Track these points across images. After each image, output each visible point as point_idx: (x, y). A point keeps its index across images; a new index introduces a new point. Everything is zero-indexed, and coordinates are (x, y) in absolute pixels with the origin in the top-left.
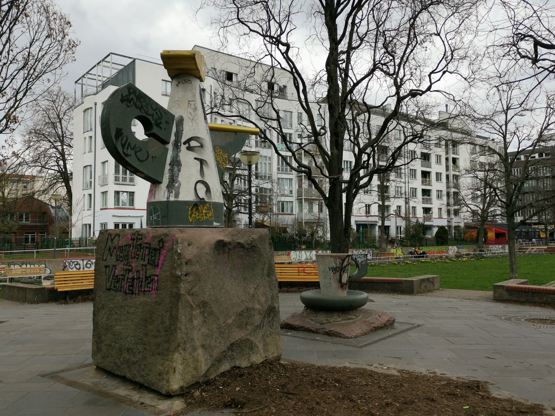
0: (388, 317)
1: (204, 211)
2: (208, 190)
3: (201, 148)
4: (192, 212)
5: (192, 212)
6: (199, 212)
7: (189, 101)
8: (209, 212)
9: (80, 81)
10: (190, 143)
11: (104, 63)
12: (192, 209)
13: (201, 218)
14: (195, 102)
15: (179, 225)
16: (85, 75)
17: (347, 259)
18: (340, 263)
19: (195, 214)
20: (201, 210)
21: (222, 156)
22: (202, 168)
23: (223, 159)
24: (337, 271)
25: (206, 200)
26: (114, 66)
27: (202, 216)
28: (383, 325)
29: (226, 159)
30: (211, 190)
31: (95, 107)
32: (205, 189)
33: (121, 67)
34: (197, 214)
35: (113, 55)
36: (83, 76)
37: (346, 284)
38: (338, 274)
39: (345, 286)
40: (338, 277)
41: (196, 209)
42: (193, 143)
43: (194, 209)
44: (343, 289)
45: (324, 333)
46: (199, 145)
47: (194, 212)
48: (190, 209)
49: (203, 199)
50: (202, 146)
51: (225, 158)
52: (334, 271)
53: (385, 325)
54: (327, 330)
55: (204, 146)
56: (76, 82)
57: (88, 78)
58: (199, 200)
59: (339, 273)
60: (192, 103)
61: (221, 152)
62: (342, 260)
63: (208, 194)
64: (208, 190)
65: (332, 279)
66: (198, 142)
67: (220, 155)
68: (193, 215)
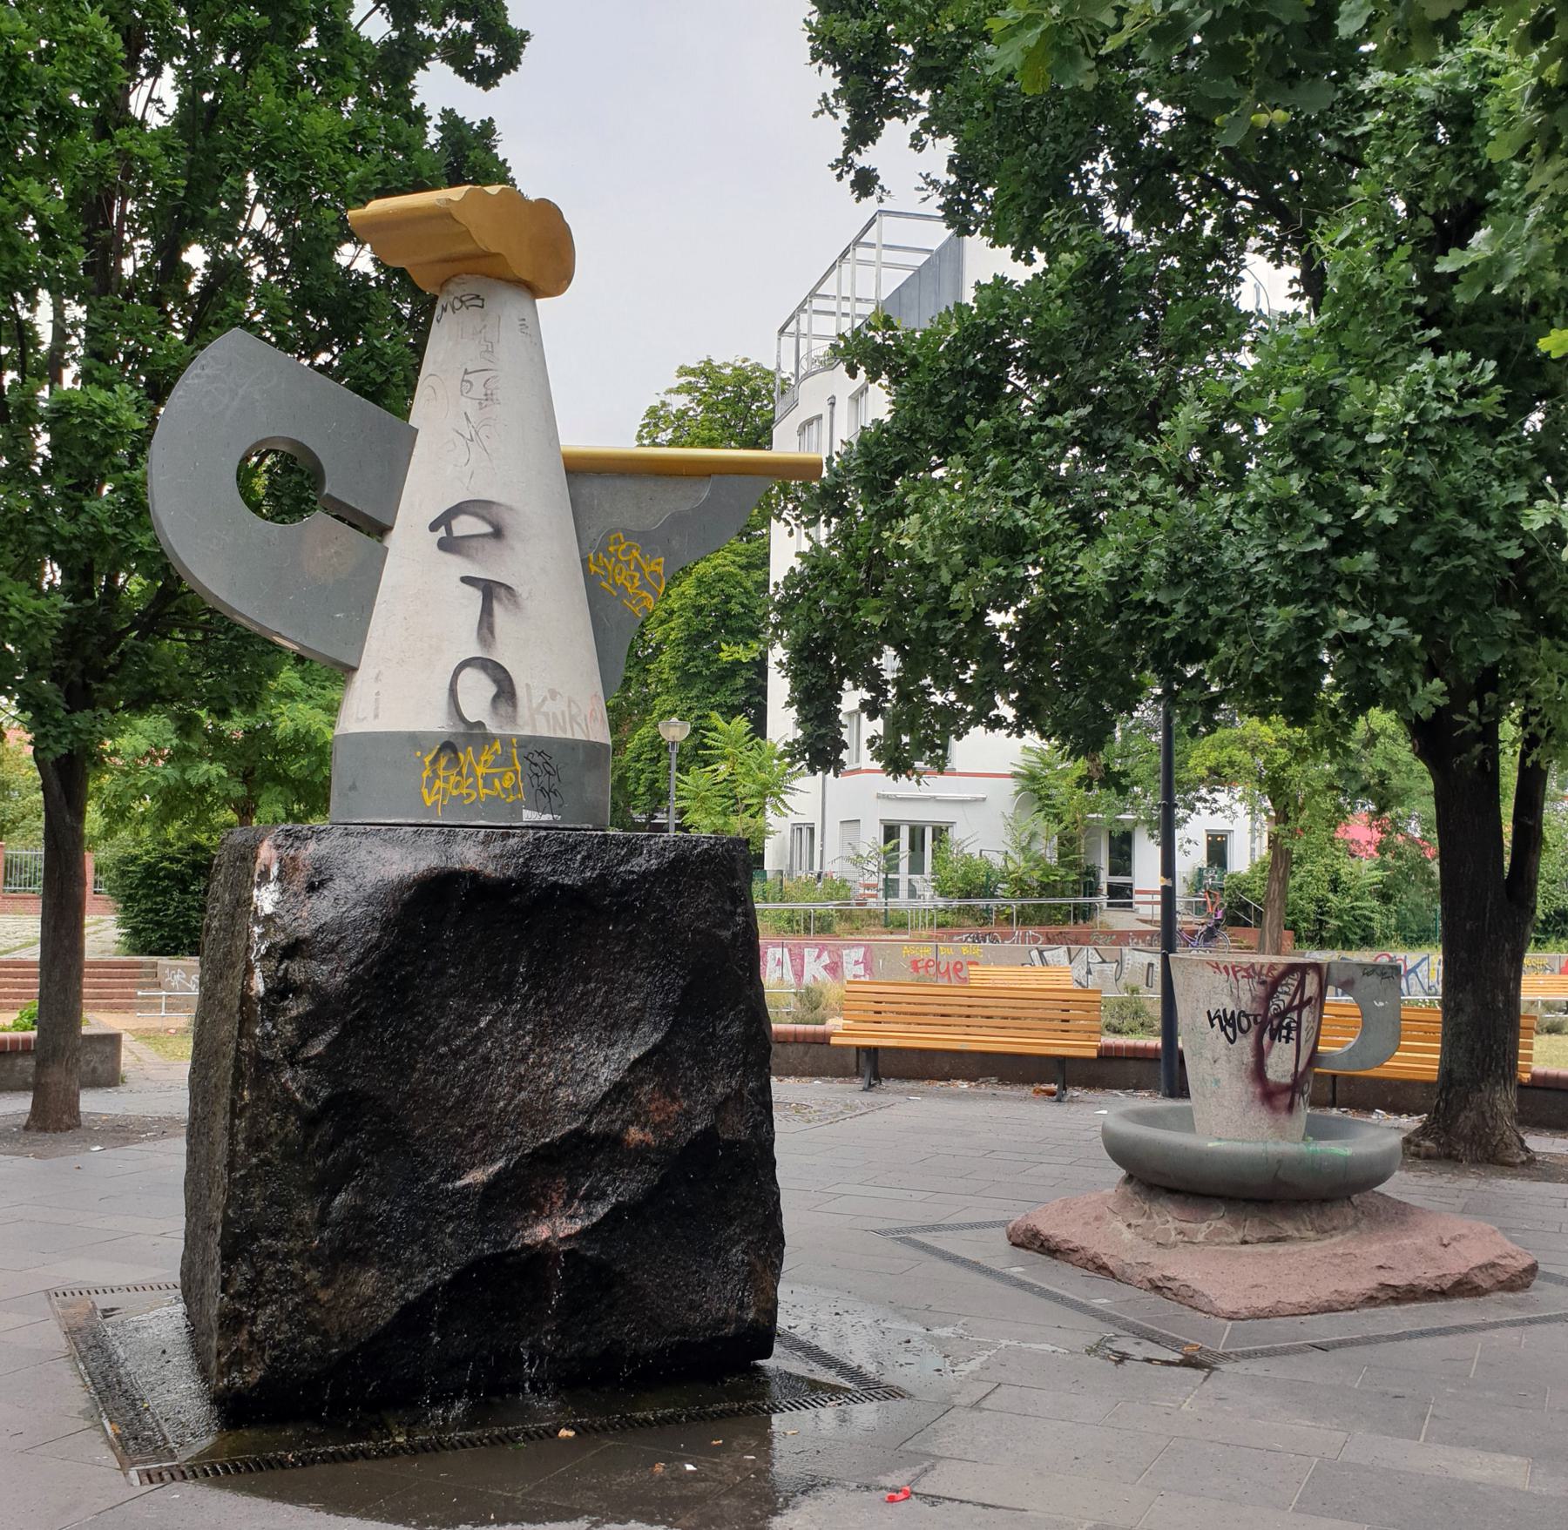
1: (480, 770)
2: (505, 691)
3: (490, 544)
4: (434, 771)
6: (460, 773)
7: (466, 372)
8: (503, 773)
9: (791, 328)
10: (455, 523)
11: (861, 253)
12: (435, 760)
13: (469, 795)
14: (487, 375)
15: (390, 817)
17: (1293, 981)
18: (1254, 999)
19: (446, 779)
20: (470, 764)
21: (638, 568)
22: (487, 612)
23: (642, 578)
24: (1243, 1031)
25: (492, 728)
26: (888, 255)
27: (474, 786)
28: (1447, 1284)
29: (658, 579)
30: (520, 691)
31: (832, 413)
32: (492, 690)
33: (920, 259)
34: (453, 779)
35: (886, 219)
36: (801, 309)
38: (1246, 1043)
40: (1249, 1058)
41: (449, 761)
42: (465, 526)
43: (443, 762)
44: (1274, 1109)
46: (487, 529)
47: (441, 773)
48: (428, 760)
49: (480, 724)
50: (498, 533)
51: (652, 573)
52: (1229, 1030)
53: (1459, 1283)
54: (1154, 1275)
55: (507, 532)
56: (782, 331)
57: (816, 312)
58: (461, 729)
59: (1251, 1037)
61: (636, 554)
62: (1263, 983)
63: (504, 708)
64: (505, 691)
65: (1223, 1061)
66: (483, 518)
67: (628, 563)
68: (439, 784)
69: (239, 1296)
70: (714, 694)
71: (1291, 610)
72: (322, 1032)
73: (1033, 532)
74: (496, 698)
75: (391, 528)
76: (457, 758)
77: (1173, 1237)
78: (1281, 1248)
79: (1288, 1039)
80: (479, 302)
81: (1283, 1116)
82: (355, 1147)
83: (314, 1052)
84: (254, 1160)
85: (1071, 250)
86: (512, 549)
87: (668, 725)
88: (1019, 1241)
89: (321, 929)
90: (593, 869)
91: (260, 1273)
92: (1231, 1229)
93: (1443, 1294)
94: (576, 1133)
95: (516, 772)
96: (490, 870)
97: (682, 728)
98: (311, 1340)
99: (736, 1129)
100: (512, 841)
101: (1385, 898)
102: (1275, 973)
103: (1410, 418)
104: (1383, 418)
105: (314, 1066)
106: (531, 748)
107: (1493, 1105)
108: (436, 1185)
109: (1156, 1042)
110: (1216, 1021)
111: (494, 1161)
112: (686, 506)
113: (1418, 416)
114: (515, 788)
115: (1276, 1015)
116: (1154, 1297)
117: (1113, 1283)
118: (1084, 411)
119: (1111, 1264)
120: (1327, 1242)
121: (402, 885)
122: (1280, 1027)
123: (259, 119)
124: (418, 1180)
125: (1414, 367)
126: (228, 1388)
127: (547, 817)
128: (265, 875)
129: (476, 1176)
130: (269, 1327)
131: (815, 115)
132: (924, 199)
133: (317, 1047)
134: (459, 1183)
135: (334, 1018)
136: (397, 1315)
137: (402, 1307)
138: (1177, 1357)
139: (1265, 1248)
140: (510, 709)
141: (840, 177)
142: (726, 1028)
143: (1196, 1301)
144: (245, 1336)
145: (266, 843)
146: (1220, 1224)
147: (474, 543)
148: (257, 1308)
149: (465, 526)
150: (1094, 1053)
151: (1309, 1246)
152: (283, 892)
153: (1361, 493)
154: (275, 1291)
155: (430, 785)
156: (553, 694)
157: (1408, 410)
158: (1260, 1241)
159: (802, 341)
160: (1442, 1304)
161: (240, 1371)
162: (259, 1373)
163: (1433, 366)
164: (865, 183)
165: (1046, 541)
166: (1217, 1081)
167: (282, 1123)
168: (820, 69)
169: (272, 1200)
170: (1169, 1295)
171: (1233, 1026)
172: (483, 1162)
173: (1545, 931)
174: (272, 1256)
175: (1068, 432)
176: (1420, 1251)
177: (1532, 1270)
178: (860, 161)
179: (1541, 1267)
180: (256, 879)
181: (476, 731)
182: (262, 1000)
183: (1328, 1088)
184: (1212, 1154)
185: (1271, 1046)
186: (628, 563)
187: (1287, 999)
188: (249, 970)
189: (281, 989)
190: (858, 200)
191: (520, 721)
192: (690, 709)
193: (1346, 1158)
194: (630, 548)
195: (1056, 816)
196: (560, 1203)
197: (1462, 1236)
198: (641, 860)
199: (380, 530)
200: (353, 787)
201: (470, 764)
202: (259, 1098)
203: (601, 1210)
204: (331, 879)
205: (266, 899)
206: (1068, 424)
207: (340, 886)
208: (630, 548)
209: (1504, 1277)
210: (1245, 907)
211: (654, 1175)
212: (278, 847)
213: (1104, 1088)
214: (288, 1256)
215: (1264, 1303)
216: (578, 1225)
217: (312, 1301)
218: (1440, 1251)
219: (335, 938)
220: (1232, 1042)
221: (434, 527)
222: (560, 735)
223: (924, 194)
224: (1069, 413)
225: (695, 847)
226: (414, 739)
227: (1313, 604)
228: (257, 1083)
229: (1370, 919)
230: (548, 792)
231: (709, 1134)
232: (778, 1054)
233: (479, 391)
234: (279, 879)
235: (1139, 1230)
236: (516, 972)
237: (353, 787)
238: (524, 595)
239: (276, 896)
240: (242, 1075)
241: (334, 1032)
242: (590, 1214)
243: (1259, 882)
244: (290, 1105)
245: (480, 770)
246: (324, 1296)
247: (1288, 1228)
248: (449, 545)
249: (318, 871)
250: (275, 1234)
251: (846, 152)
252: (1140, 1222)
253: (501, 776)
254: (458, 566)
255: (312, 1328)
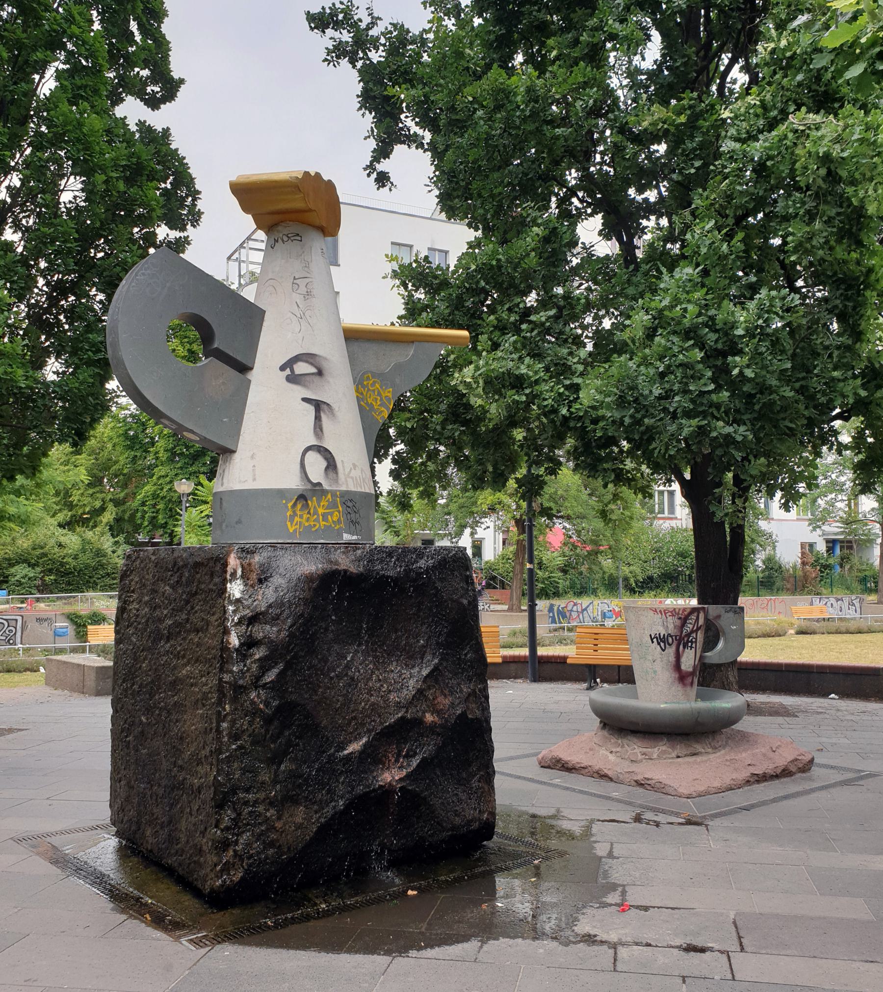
0: (797, 753)
1: (321, 511)
2: (331, 465)
3: (316, 379)
4: (294, 512)
5: (294, 512)
6: (309, 513)
7: (295, 279)
9: (234, 257)
10: (295, 367)
12: (295, 505)
13: (315, 525)
14: (307, 280)
15: (266, 539)
16: (244, 242)
17: (694, 617)
18: (675, 627)
19: (301, 516)
20: (315, 507)
21: (379, 394)
22: (318, 418)
23: (381, 400)
24: (670, 645)
25: (326, 486)
27: (317, 520)
28: (779, 771)
32: (324, 464)
34: (305, 516)
36: (241, 246)
37: (692, 674)
38: (671, 651)
39: (689, 680)
40: (672, 659)
41: (303, 506)
42: (301, 368)
43: (299, 506)
44: (684, 685)
45: (634, 783)
46: (314, 370)
47: (298, 513)
48: (290, 505)
49: (319, 484)
50: (320, 373)
51: (386, 397)
52: (662, 644)
53: (784, 770)
54: (639, 777)
55: (324, 372)
56: (229, 258)
57: (251, 249)
58: (309, 487)
59: (674, 647)
60: (302, 283)
61: (377, 386)
62: (680, 618)
63: (331, 474)
64: (331, 465)
66: (312, 364)
67: (374, 391)
68: (297, 519)
69: (227, 829)
70: (191, 465)
71: (695, 422)
72: (273, 667)
73: (529, 378)
74: (327, 469)
75: (251, 369)
76: (307, 505)
77: (640, 757)
78: (699, 759)
79: (691, 647)
80: (299, 238)
81: (689, 688)
82: (289, 735)
83: (270, 679)
84: (234, 747)
85: (538, 226)
86: (328, 382)
87: (181, 484)
88: (546, 765)
89: (270, 606)
90: (401, 567)
91: (239, 814)
92: (670, 750)
93: (777, 777)
94: (402, 718)
95: (339, 512)
96: (353, 569)
97: (188, 486)
98: (271, 851)
99: (474, 713)
100: (359, 552)
101: (564, 571)
102: (686, 613)
103: (760, 322)
104: (745, 322)
105: (269, 688)
106: (346, 498)
107: (727, 678)
108: (333, 754)
109: (525, 652)
110: (655, 640)
111: (361, 738)
112: (402, 360)
113: (764, 322)
114: (339, 521)
115: (686, 636)
116: (641, 790)
117: (612, 784)
118: (552, 312)
119: (610, 773)
120: (718, 754)
121: (309, 579)
122: (688, 641)
123: (58, 118)
124: (324, 752)
125: (758, 296)
126: (222, 886)
127: (355, 537)
128: (234, 574)
129: (354, 747)
130: (248, 845)
131: (365, 139)
132: (430, 191)
133: (271, 676)
134: (346, 752)
135: (281, 658)
136: (316, 833)
137: (318, 827)
138: (683, 821)
139: (691, 759)
140: (335, 475)
141: (369, 175)
142: (466, 655)
143: (667, 790)
144: (231, 853)
145: (232, 556)
146: (664, 748)
147: (308, 378)
148: (237, 835)
149: (301, 368)
150: (500, 660)
151: (711, 756)
152: (246, 585)
153: (735, 361)
154: (248, 824)
155: (292, 521)
156: (355, 466)
157: (759, 318)
158: (686, 756)
159: (242, 264)
160: (777, 782)
161: (229, 874)
162: (240, 875)
163: (769, 295)
164: (383, 179)
165: (537, 382)
166: (655, 672)
167: (251, 723)
168: (363, 115)
169: (244, 771)
170: (649, 788)
171: (664, 642)
172: (356, 739)
173: (642, 587)
174: (246, 803)
175: (543, 324)
176: (764, 755)
177: (812, 761)
178: (381, 167)
179: (816, 761)
180: (228, 577)
181: (317, 488)
182: (237, 650)
183: (616, 674)
184: (663, 711)
185: (684, 651)
186: (374, 391)
187: (691, 626)
188: (226, 632)
189: (249, 643)
190: (378, 189)
191: (340, 482)
192: (176, 475)
193: (729, 709)
194: (374, 383)
195: (395, 532)
196: (393, 760)
197: (780, 746)
198: (423, 561)
199: (244, 368)
200: (239, 522)
201: (315, 507)
202: (236, 709)
203: (415, 762)
204: (271, 576)
205: (235, 589)
206: (543, 319)
207: (277, 580)
208: (374, 383)
209: (801, 765)
210: (494, 578)
211: (439, 740)
212: (239, 558)
213: (498, 679)
214: (256, 802)
215: (702, 788)
216: (404, 772)
217: (272, 828)
218: (772, 755)
219: (279, 611)
220: (663, 650)
221: (282, 368)
222: (359, 490)
223: (429, 188)
224: (542, 314)
225: (449, 552)
226: (281, 493)
227: (704, 418)
228: (234, 700)
229: (558, 583)
230: (354, 523)
231: (463, 715)
232: (490, 669)
233: (303, 289)
234: (242, 577)
235: (618, 754)
236: (362, 626)
237: (239, 522)
238: (337, 409)
239: (242, 587)
240: (224, 696)
241: (281, 666)
242: (409, 765)
243: (501, 565)
244: (255, 712)
245: (321, 511)
246: (279, 825)
247: (699, 748)
248: (293, 379)
249: (263, 572)
250: (247, 790)
251: (371, 162)
252: (618, 749)
253: (331, 514)
254: (301, 392)
255: (272, 844)
